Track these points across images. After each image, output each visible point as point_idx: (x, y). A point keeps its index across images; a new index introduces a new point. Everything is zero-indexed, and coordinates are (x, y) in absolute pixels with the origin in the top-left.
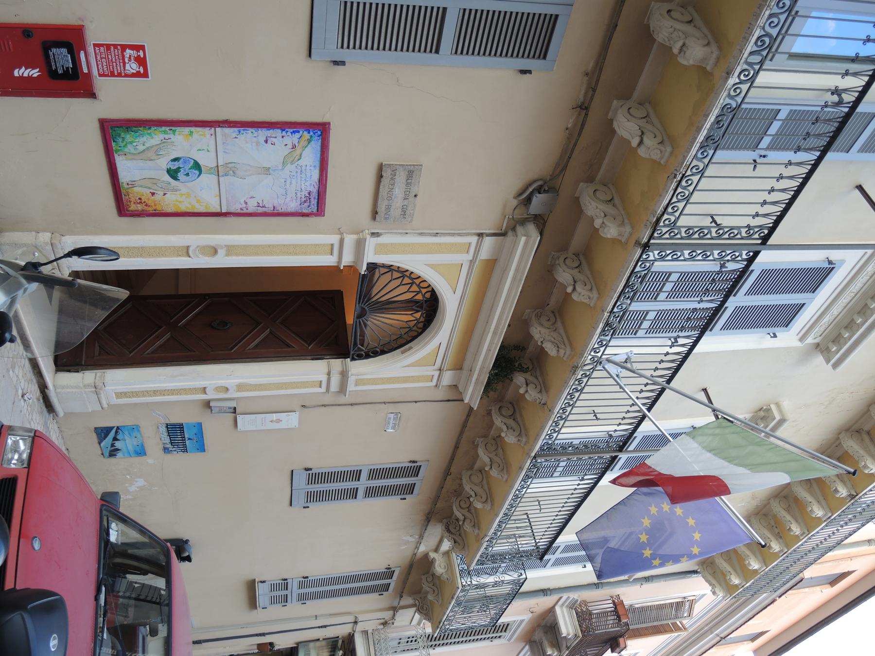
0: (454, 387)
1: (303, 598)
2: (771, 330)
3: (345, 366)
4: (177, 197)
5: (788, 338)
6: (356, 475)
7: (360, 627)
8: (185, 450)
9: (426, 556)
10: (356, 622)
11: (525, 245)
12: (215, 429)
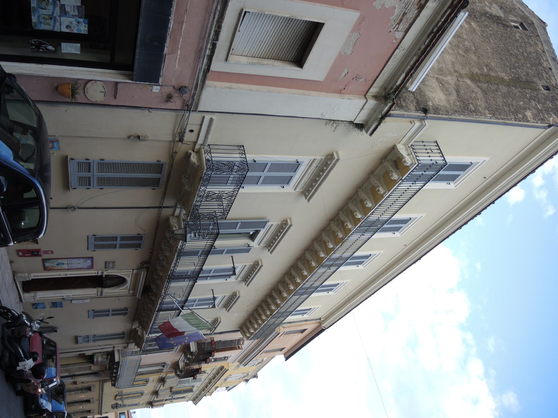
0: (134, 293)
1: (94, 341)
2: (282, 185)
3: (102, 290)
4: (60, 267)
5: (289, 189)
6: (115, 238)
7: (115, 349)
8: (57, 307)
9: (135, 329)
10: (114, 347)
11: (143, 274)
12: (64, 303)
